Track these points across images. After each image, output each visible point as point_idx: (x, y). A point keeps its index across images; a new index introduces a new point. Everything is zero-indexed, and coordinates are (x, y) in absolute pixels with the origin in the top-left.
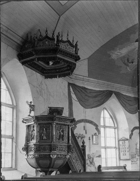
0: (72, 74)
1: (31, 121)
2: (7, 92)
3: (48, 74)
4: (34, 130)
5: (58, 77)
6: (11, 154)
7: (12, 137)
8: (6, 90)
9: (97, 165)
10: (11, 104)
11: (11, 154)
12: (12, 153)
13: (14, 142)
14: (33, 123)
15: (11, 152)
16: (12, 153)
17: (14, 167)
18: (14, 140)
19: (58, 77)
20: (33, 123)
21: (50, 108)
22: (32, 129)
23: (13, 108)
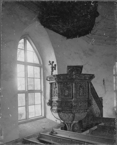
0: (90, 33)
1: (53, 79)
2: (35, 53)
3: (69, 35)
4: (56, 87)
5: (78, 37)
6: (24, 78)
7: (41, 91)
8: (33, 52)
9: (56, 102)
10: (39, 63)
11: (40, 105)
12: (41, 104)
13: (42, 95)
14: (55, 81)
15: (40, 103)
16: (41, 104)
17: (43, 115)
18: (43, 94)
19: (78, 37)
20: (55, 81)
21: (69, 67)
22: (54, 86)
23: (40, 67)
